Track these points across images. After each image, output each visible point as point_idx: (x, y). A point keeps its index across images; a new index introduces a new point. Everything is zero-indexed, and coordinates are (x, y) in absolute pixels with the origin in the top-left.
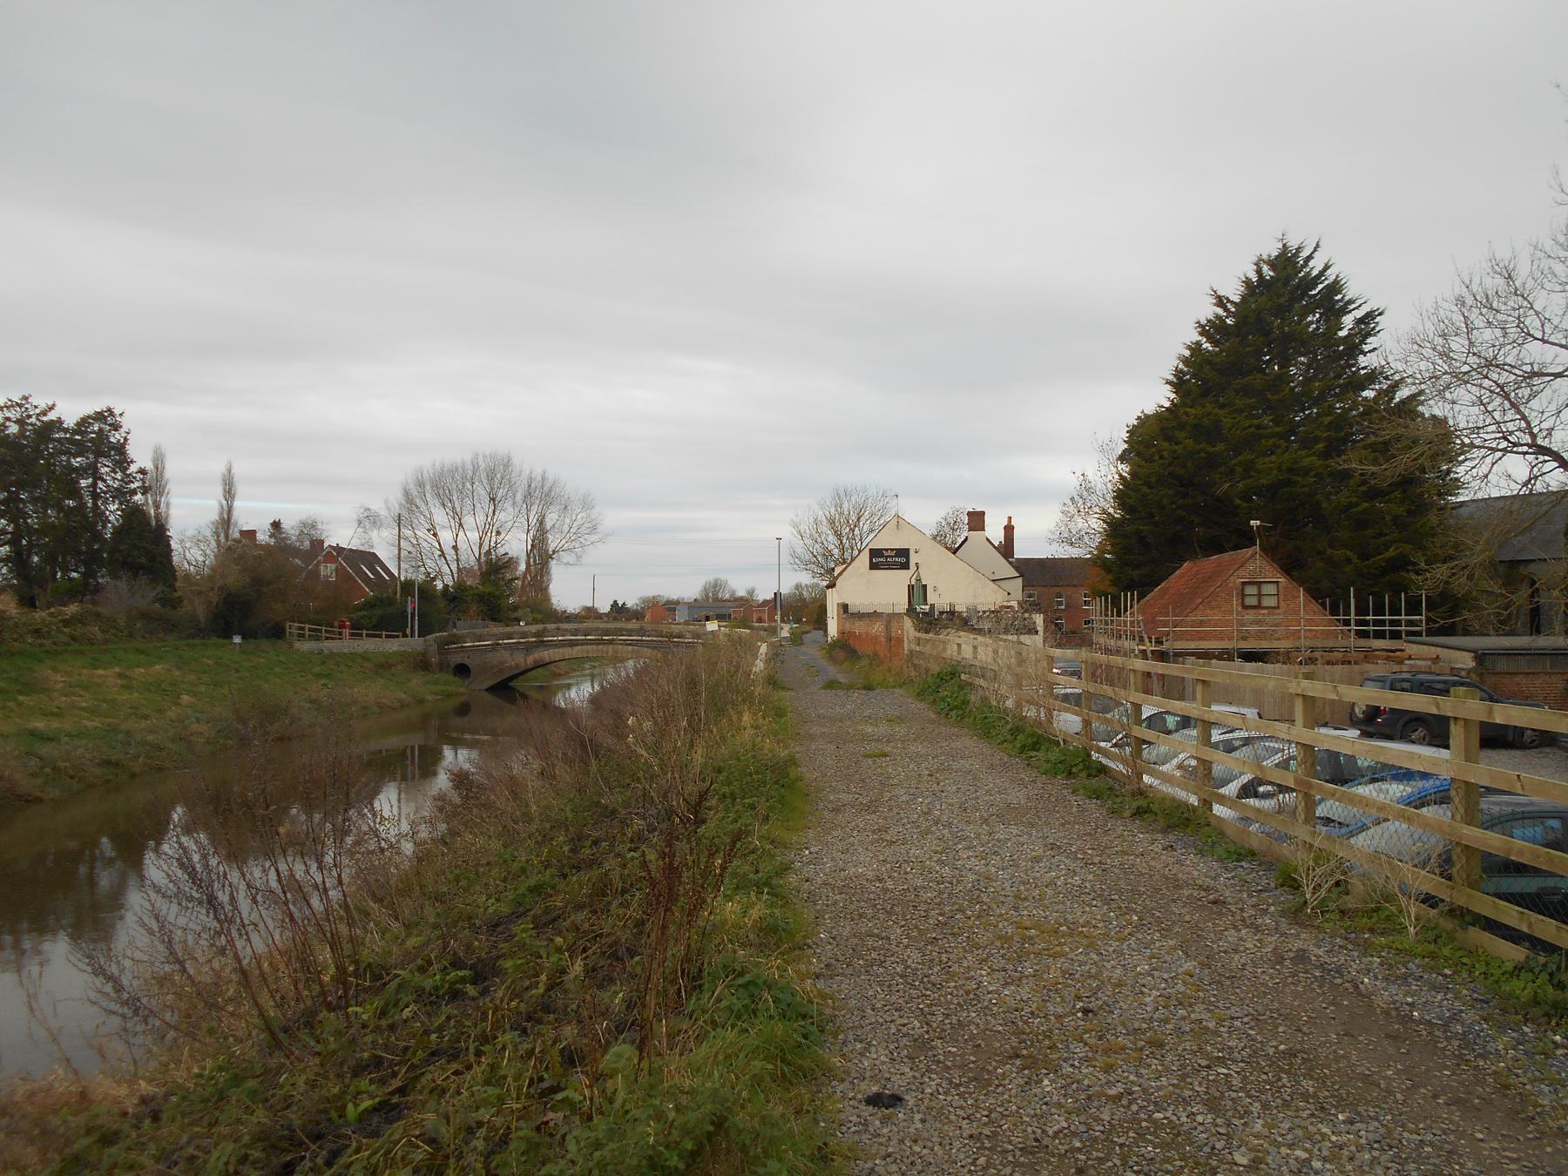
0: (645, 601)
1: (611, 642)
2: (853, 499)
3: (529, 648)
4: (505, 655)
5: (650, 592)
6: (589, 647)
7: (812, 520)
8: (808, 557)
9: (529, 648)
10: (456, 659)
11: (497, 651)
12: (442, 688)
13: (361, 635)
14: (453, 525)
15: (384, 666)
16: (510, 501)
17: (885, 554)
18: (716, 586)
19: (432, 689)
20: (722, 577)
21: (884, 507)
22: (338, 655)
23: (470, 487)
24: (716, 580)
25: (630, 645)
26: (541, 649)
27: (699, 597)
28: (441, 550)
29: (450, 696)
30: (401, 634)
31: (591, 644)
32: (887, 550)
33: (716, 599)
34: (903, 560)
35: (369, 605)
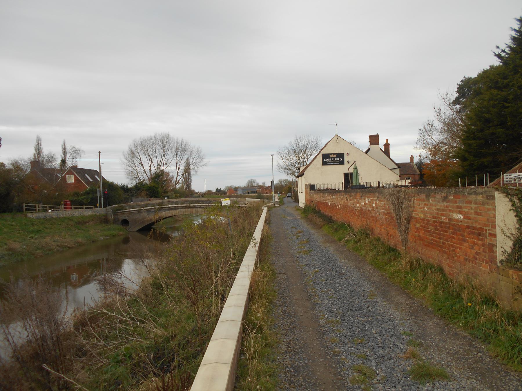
0: (227, 188)
1: (194, 207)
2: (303, 141)
3: (155, 211)
4: (144, 215)
5: (229, 185)
6: (184, 210)
7: (286, 151)
8: (285, 166)
9: (155, 211)
10: (122, 217)
11: (141, 213)
12: (112, 233)
13: (71, 208)
14: (149, 161)
15: (81, 223)
16: (170, 151)
17: (331, 156)
18: (252, 182)
19: (118, 230)
20: (254, 178)
21: (317, 144)
22: (56, 219)
23: (154, 146)
24: (252, 180)
25: (203, 208)
26: (162, 211)
27: (246, 186)
28: (145, 171)
29: (114, 236)
30: (94, 206)
31: (185, 208)
32: (331, 154)
33: (252, 186)
34: (341, 159)
35: (87, 193)
